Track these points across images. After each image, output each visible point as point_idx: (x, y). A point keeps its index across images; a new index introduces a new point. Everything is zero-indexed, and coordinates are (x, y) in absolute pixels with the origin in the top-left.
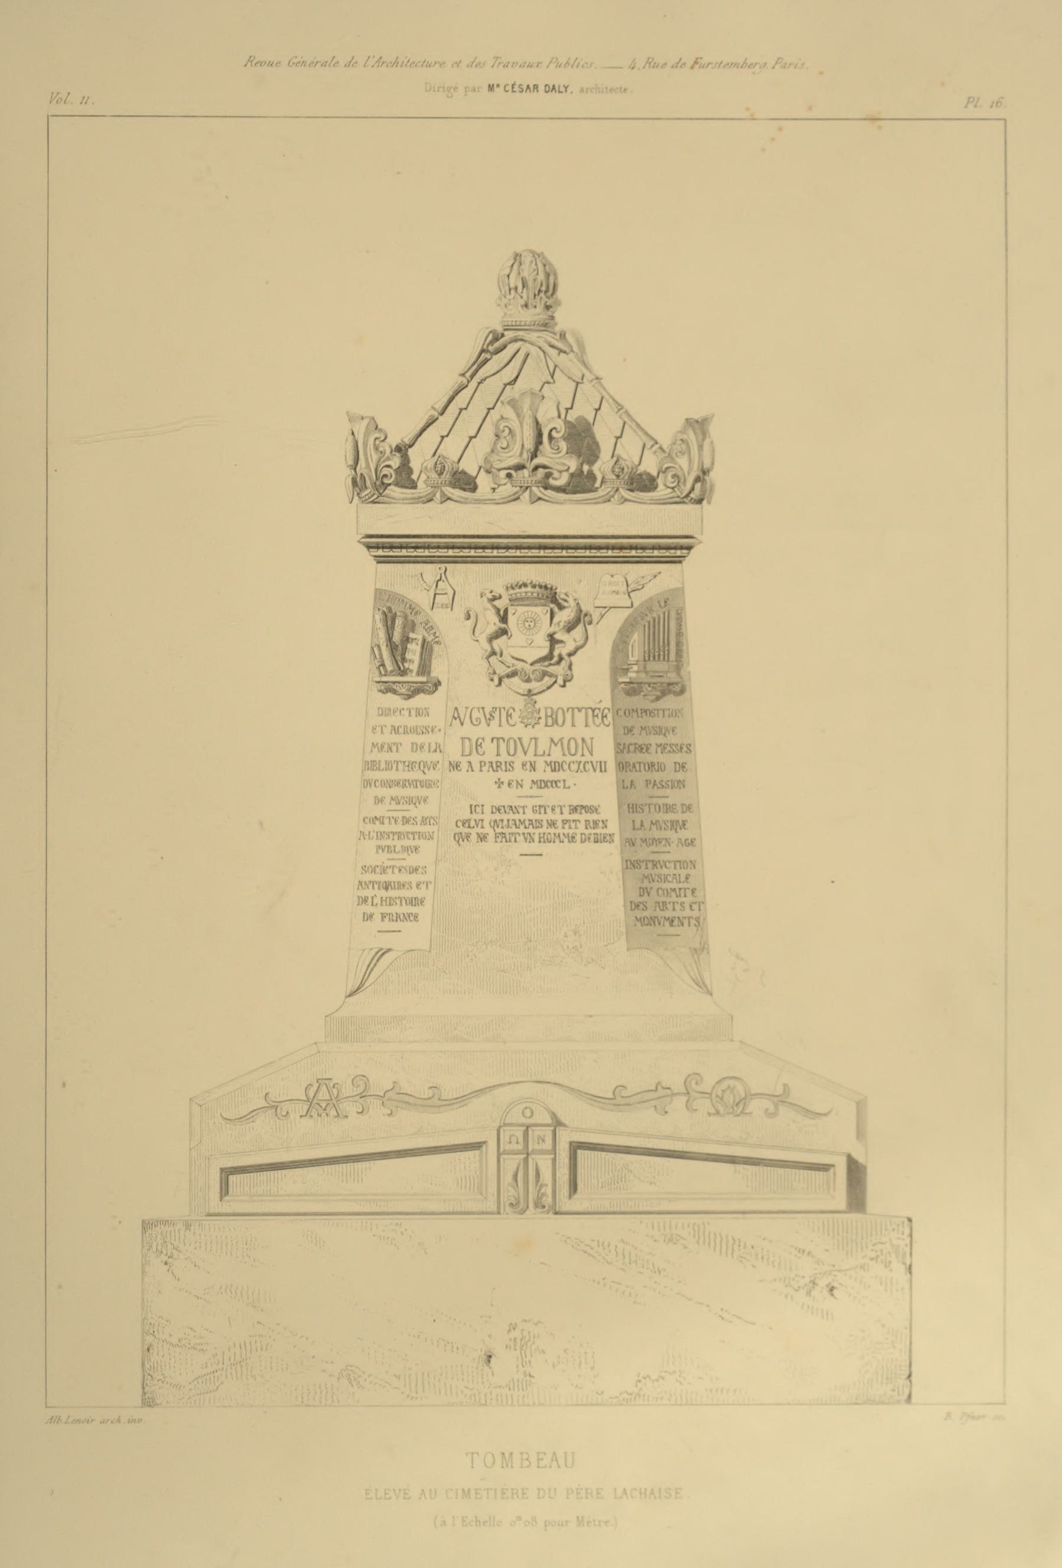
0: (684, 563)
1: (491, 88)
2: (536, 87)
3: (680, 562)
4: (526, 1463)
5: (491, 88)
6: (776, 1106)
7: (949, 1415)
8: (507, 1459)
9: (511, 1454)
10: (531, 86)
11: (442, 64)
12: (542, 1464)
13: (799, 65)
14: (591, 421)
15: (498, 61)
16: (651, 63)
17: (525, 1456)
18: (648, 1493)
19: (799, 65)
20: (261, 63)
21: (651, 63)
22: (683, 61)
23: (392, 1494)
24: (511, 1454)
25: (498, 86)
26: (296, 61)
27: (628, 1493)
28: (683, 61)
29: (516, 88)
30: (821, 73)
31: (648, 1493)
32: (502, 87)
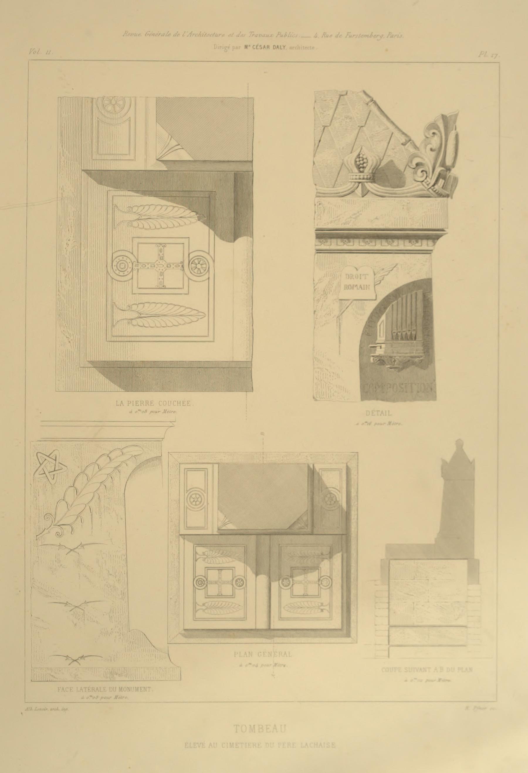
0: (432, 254)
1: (246, 47)
2: (268, 47)
3: (430, 253)
4: (261, 730)
5: (246, 47)
6: (206, 577)
7: (467, 708)
8: (252, 729)
9: (254, 725)
10: (266, 46)
11: (223, 35)
12: (268, 730)
13: (400, 36)
14: (403, 171)
15: (252, 34)
16: (325, 35)
17: (261, 727)
18: (319, 744)
19: (400, 36)
20: (131, 35)
21: (325, 35)
22: (340, 34)
23: (197, 745)
24: (254, 725)
25: (249, 46)
26: (149, 33)
27: (309, 745)
28: (340, 34)
29: (258, 47)
30: (387, 50)
31: (319, 744)
32: (252, 46)
